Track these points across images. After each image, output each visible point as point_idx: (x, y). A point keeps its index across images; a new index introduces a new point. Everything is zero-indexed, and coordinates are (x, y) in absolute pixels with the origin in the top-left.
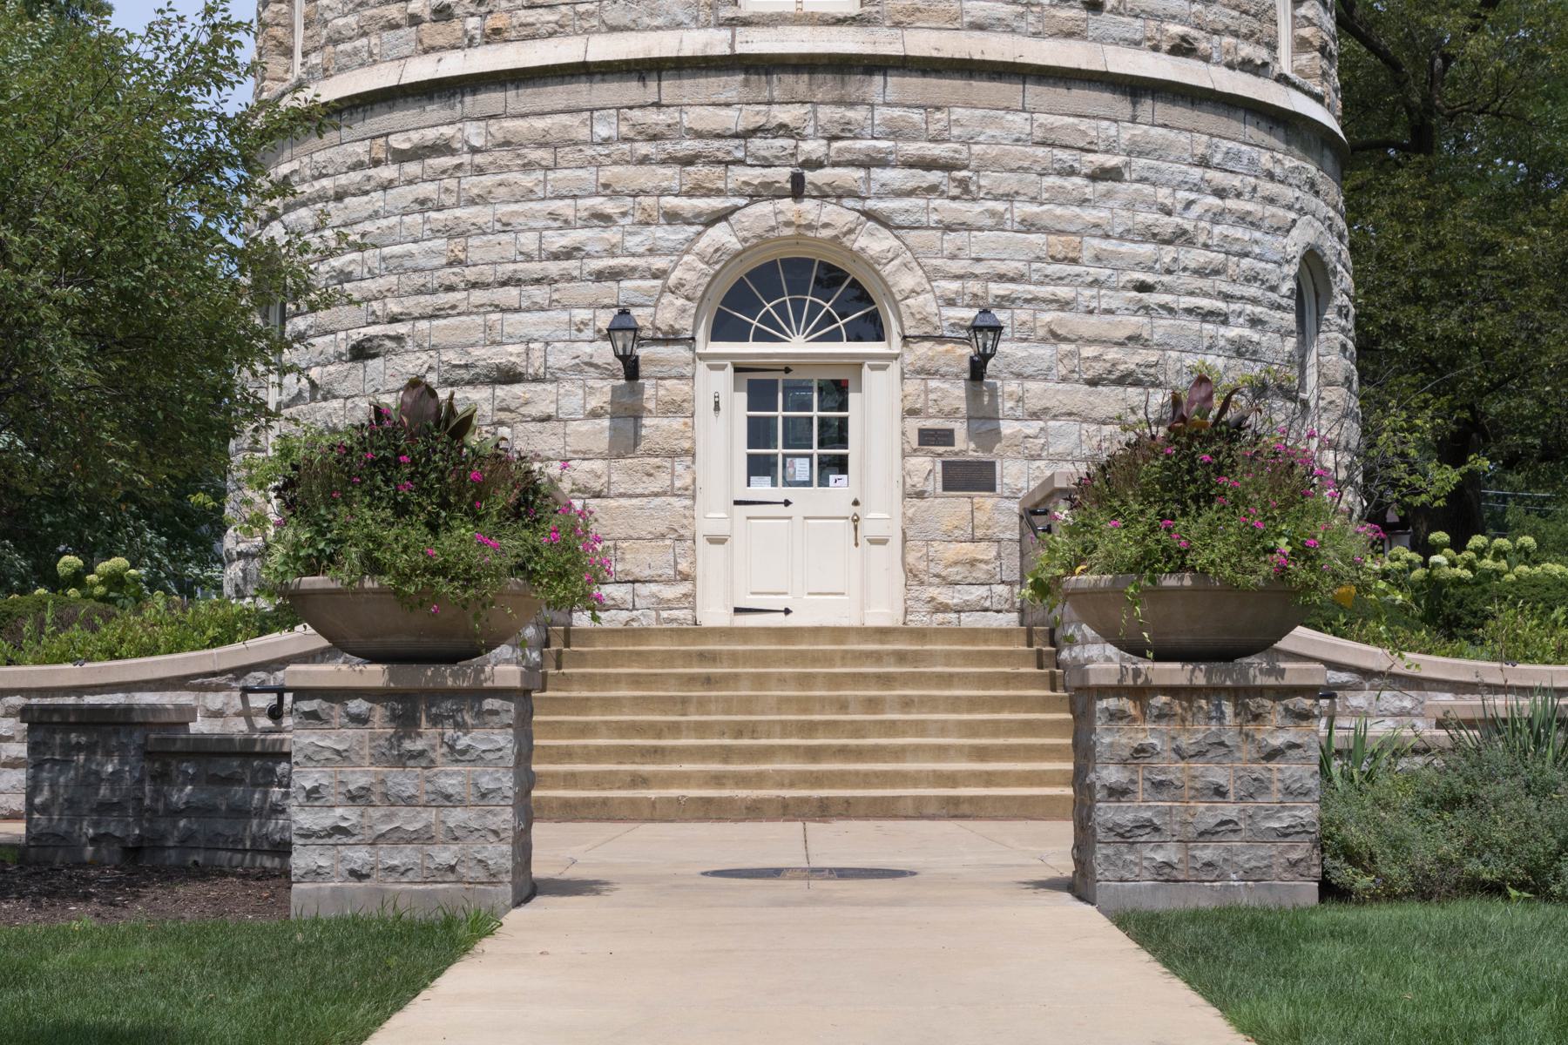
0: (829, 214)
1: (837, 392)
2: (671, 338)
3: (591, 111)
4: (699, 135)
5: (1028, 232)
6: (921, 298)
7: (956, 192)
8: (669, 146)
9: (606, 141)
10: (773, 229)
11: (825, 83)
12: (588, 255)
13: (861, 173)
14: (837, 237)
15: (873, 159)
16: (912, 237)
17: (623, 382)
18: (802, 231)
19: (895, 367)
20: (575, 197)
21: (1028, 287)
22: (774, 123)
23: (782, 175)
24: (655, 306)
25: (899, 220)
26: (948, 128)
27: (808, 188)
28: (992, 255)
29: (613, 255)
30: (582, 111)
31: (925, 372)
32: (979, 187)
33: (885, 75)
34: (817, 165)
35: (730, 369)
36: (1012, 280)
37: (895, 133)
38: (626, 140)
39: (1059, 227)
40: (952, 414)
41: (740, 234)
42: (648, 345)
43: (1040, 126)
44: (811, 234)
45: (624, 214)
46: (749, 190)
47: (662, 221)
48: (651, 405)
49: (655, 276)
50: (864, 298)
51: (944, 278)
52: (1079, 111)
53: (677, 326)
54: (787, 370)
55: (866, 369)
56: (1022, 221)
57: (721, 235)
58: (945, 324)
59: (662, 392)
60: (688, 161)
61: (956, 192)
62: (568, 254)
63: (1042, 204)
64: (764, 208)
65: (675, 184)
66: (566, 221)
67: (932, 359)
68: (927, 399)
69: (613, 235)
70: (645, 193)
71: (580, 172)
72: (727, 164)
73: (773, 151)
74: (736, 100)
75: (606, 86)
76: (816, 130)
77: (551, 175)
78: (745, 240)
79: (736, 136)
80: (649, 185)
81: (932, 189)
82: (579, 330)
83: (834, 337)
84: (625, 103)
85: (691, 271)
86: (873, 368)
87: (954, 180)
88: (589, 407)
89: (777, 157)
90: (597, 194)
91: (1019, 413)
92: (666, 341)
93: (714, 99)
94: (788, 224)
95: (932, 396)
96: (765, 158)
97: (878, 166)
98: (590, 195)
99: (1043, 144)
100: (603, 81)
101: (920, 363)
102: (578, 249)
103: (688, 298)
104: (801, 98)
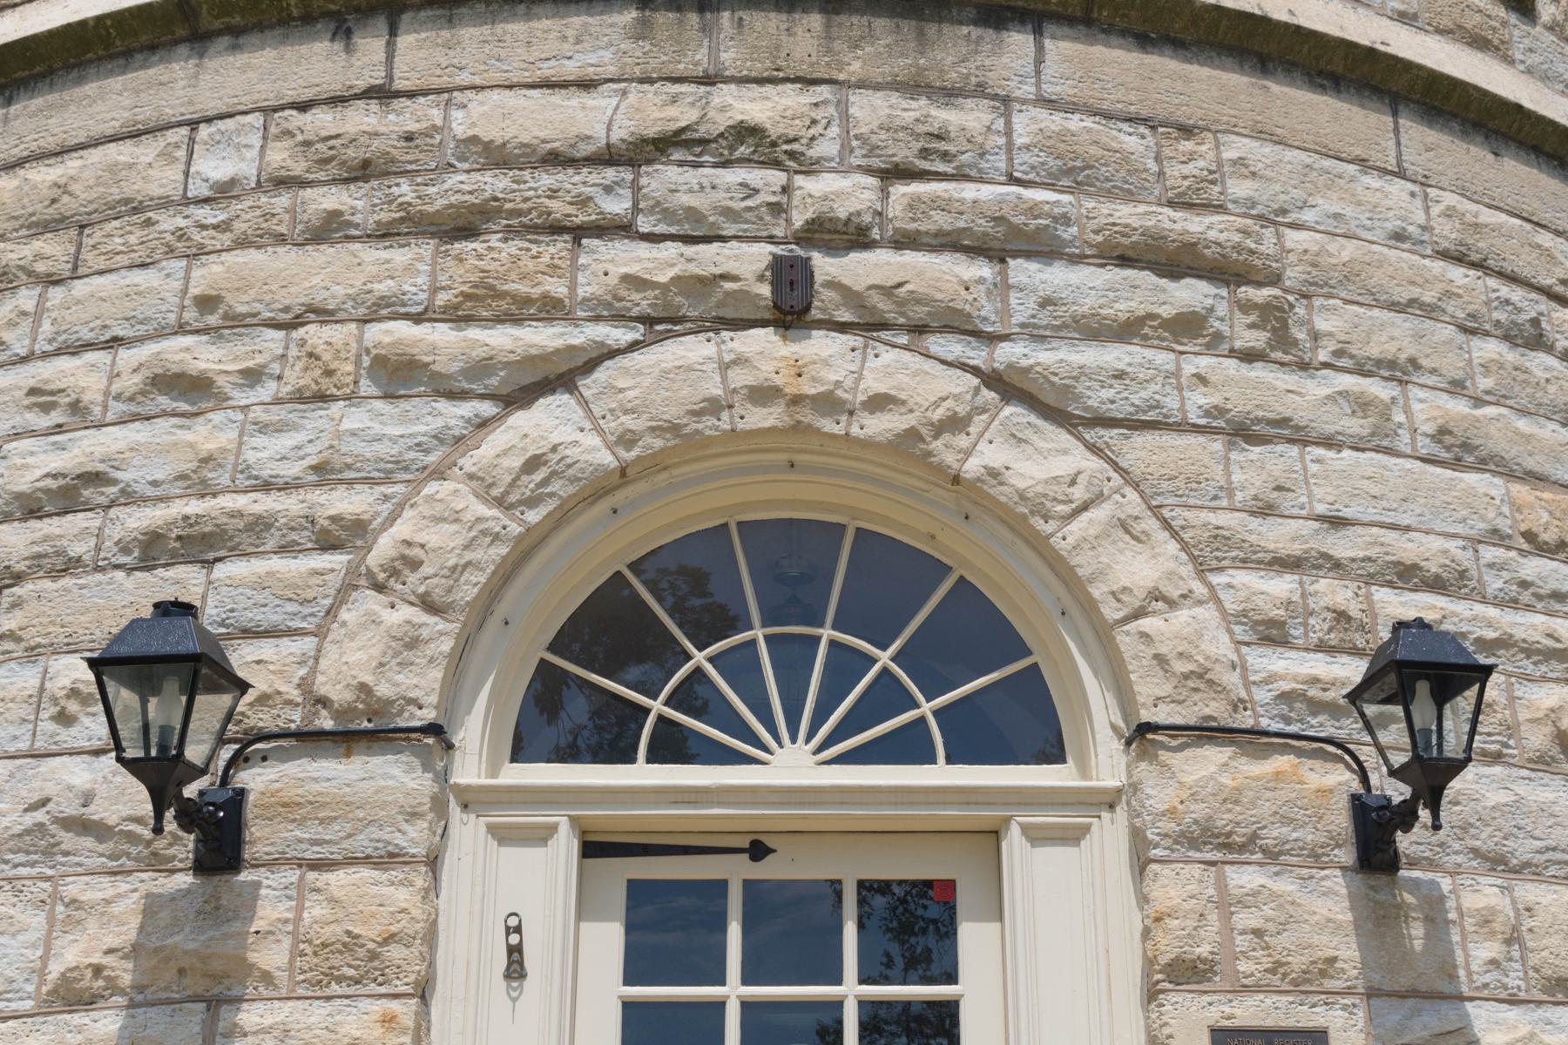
0: (887, 373)
1: (915, 925)
2: (364, 730)
3: (193, 124)
4: (497, 157)
5: (1457, 464)
6: (1183, 616)
7: (1257, 339)
8: (404, 190)
9: (224, 192)
10: (714, 407)
11: (870, 36)
12: (130, 497)
13: (983, 270)
14: (912, 434)
15: (1016, 231)
16: (1139, 450)
17: (185, 880)
18: (807, 416)
19: (1109, 836)
20: (116, 342)
21: (1479, 609)
22: (721, 122)
23: (746, 262)
24: (320, 633)
25: (1099, 397)
26: (1215, 176)
27: (824, 302)
28: (1371, 514)
29: (206, 491)
30: (170, 126)
31: (1217, 842)
32: (1316, 336)
33: (1038, 32)
34: (851, 236)
35: (565, 845)
36: (1436, 585)
37: (1074, 174)
38: (283, 182)
39: (1530, 463)
40: (1310, 980)
41: (609, 425)
42: (285, 756)
43: (1449, 213)
44: (828, 426)
45: (252, 377)
46: (643, 303)
47: (366, 387)
48: (271, 957)
49: (327, 543)
50: (1001, 640)
51: (1244, 563)
52: (1527, 209)
53: (383, 690)
54: (758, 851)
55: (1014, 844)
56: (1442, 433)
57: (549, 422)
58: (1262, 695)
59: (315, 910)
60: (461, 226)
61: (1257, 339)
62: (70, 494)
63: (1479, 402)
64: (693, 350)
65: (415, 287)
66: (76, 407)
67: (1233, 798)
68: (1228, 929)
69: (211, 433)
70: (324, 314)
71: (139, 277)
72: (579, 233)
73: (720, 197)
74: (611, 71)
75: (240, 59)
76: (847, 149)
77: (56, 294)
78: (627, 439)
79: (608, 157)
80: (336, 294)
81: (1187, 326)
82: (64, 719)
83: (908, 747)
84: (291, 95)
85: (445, 526)
86: (1037, 836)
87: (1246, 307)
88: (55, 969)
89: (728, 213)
90: (181, 329)
91: (1514, 980)
92: (346, 740)
93: (548, 70)
94: (762, 394)
95: (1245, 919)
96: (693, 214)
97: (1028, 255)
98: (161, 334)
99: (1459, 259)
100: (235, 48)
101: (1199, 810)
102: (95, 478)
103: (429, 605)
104: (804, 70)
